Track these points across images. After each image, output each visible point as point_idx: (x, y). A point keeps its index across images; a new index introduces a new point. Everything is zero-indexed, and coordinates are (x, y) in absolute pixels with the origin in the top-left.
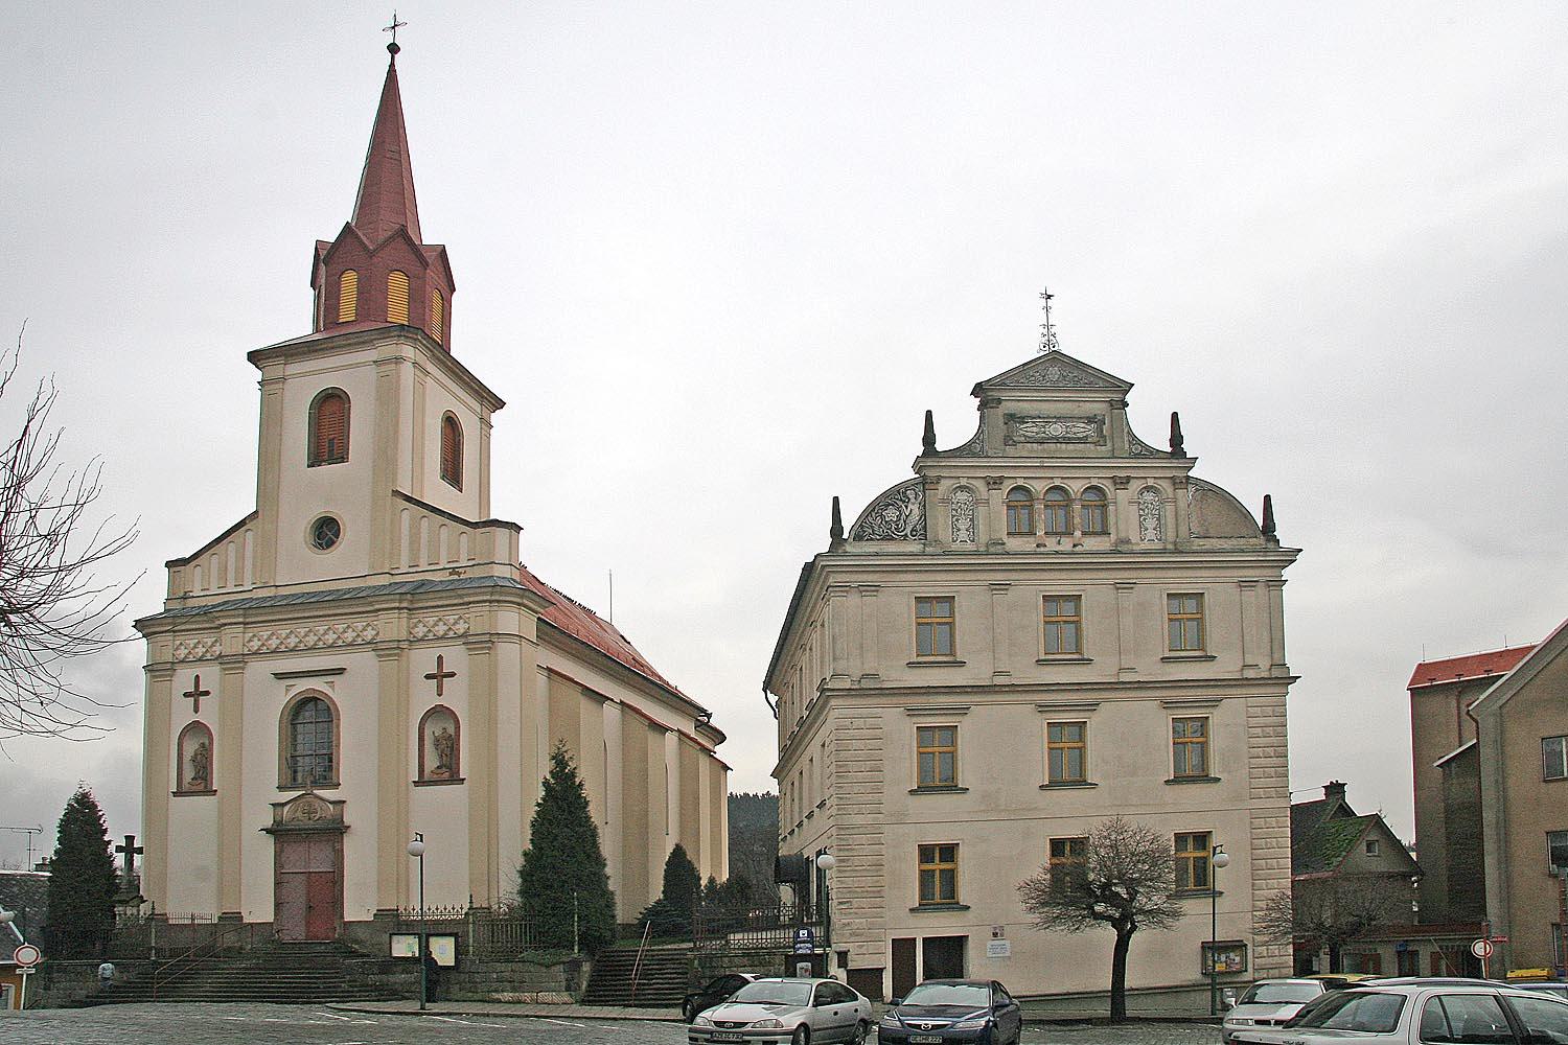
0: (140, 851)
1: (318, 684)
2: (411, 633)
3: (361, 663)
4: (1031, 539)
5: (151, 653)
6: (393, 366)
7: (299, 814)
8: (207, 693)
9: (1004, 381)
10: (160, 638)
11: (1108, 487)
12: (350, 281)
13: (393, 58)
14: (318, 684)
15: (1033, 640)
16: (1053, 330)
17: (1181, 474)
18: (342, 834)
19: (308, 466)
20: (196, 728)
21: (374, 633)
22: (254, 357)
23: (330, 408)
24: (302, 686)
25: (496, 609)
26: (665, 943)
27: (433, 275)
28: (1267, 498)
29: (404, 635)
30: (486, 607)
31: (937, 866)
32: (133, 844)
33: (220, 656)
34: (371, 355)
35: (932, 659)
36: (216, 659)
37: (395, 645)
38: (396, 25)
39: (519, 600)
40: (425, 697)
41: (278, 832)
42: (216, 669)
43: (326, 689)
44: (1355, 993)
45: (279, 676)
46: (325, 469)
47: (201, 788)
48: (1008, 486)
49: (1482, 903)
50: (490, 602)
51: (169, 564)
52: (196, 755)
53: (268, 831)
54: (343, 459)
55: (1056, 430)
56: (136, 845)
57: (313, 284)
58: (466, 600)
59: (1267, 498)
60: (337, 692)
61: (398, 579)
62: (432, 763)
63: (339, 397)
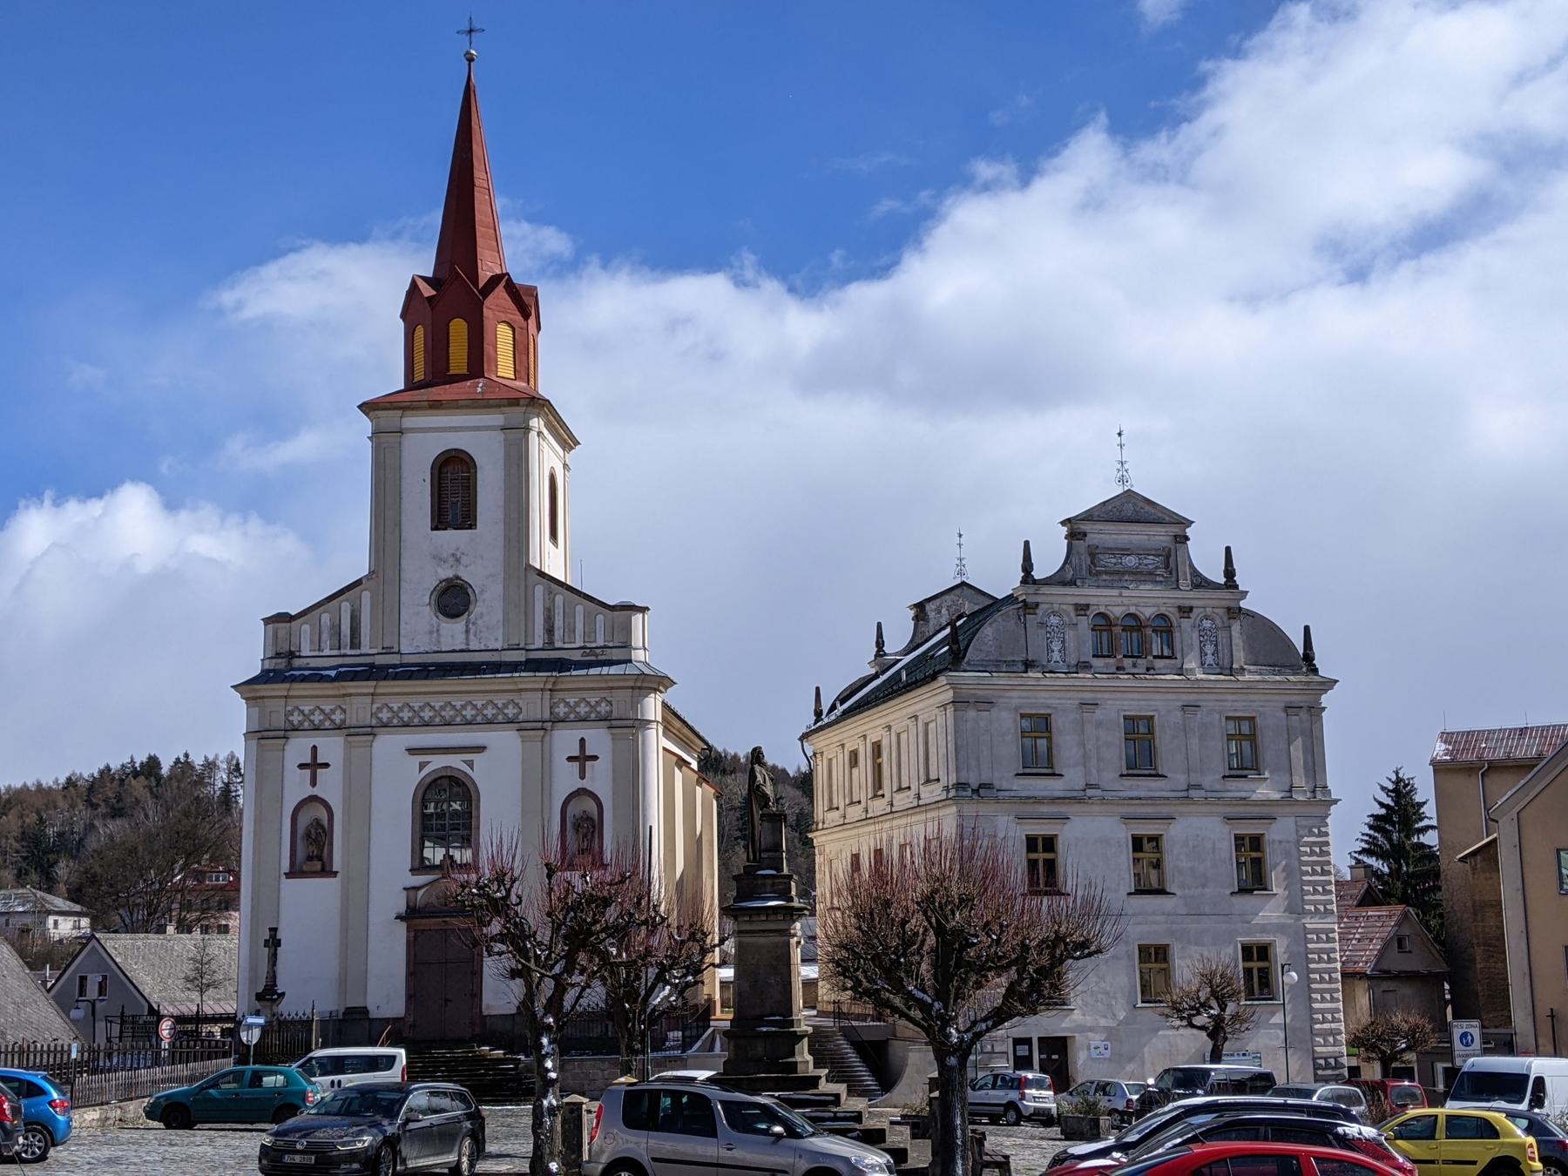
1: (456, 761)
3: (504, 744)
4: (1111, 661)
9: (1088, 516)
13: (470, 65)
15: (1009, 749)
16: (1126, 466)
17: (1232, 604)
22: (367, 407)
24: (438, 762)
28: (1307, 629)
29: (547, 715)
31: (1041, 856)
35: (1034, 771)
38: (471, 31)
40: (566, 780)
45: (412, 751)
49: (1506, 1013)
54: (472, 526)
55: (1130, 561)
59: (1307, 629)
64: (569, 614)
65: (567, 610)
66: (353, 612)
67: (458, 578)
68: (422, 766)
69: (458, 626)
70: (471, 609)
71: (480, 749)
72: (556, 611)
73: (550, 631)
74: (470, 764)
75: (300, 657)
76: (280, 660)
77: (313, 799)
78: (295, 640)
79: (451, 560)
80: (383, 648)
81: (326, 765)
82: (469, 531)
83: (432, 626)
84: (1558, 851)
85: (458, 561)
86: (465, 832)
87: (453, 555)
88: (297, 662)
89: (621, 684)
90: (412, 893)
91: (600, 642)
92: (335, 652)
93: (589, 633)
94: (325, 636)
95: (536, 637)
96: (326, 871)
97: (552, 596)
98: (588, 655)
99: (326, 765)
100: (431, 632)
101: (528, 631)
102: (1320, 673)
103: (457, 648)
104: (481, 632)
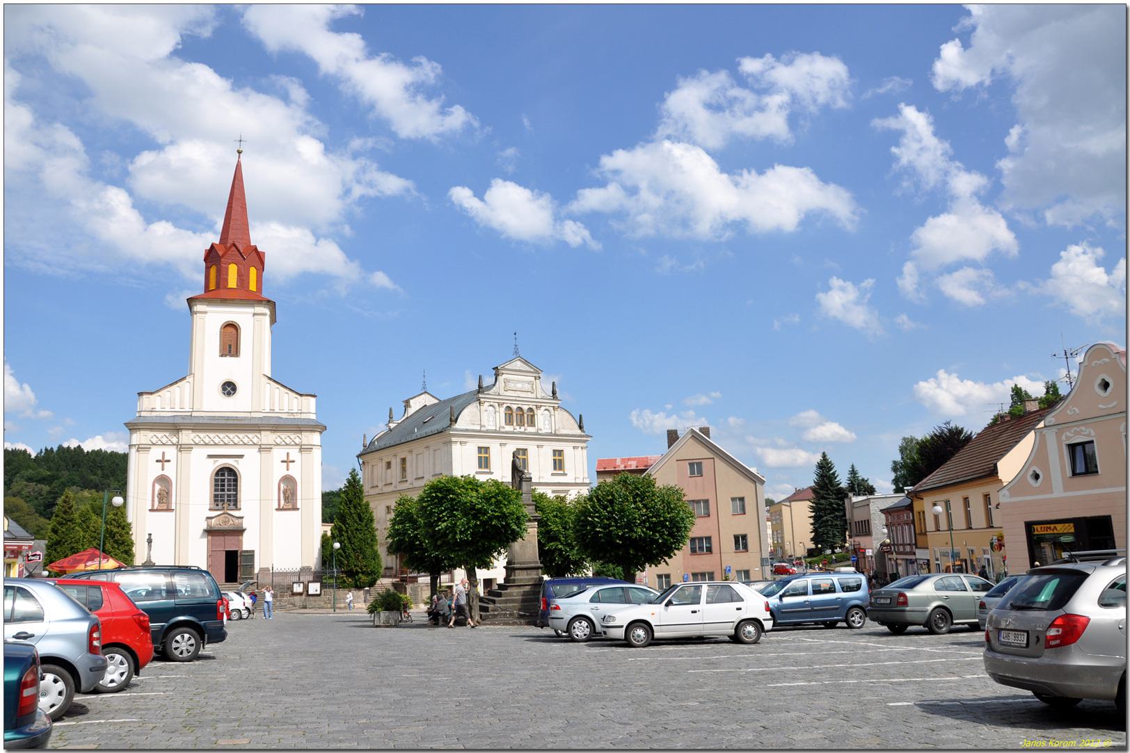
3: (251, 454)
11: (534, 408)
13: (239, 157)
24: (222, 462)
26: (360, 616)
32: (960, 40)
40: (281, 471)
41: (209, 532)
43: (235, 464)
45: (210, 456)
47: (165, 507)
48: (505, 406)
59: (580, 416)
60: (239, 466)
71: (241, 456)
84: (1028, 632)
86: (234, 493)
89: (744, 471)
90: (209, 520)
102: (776, 501)
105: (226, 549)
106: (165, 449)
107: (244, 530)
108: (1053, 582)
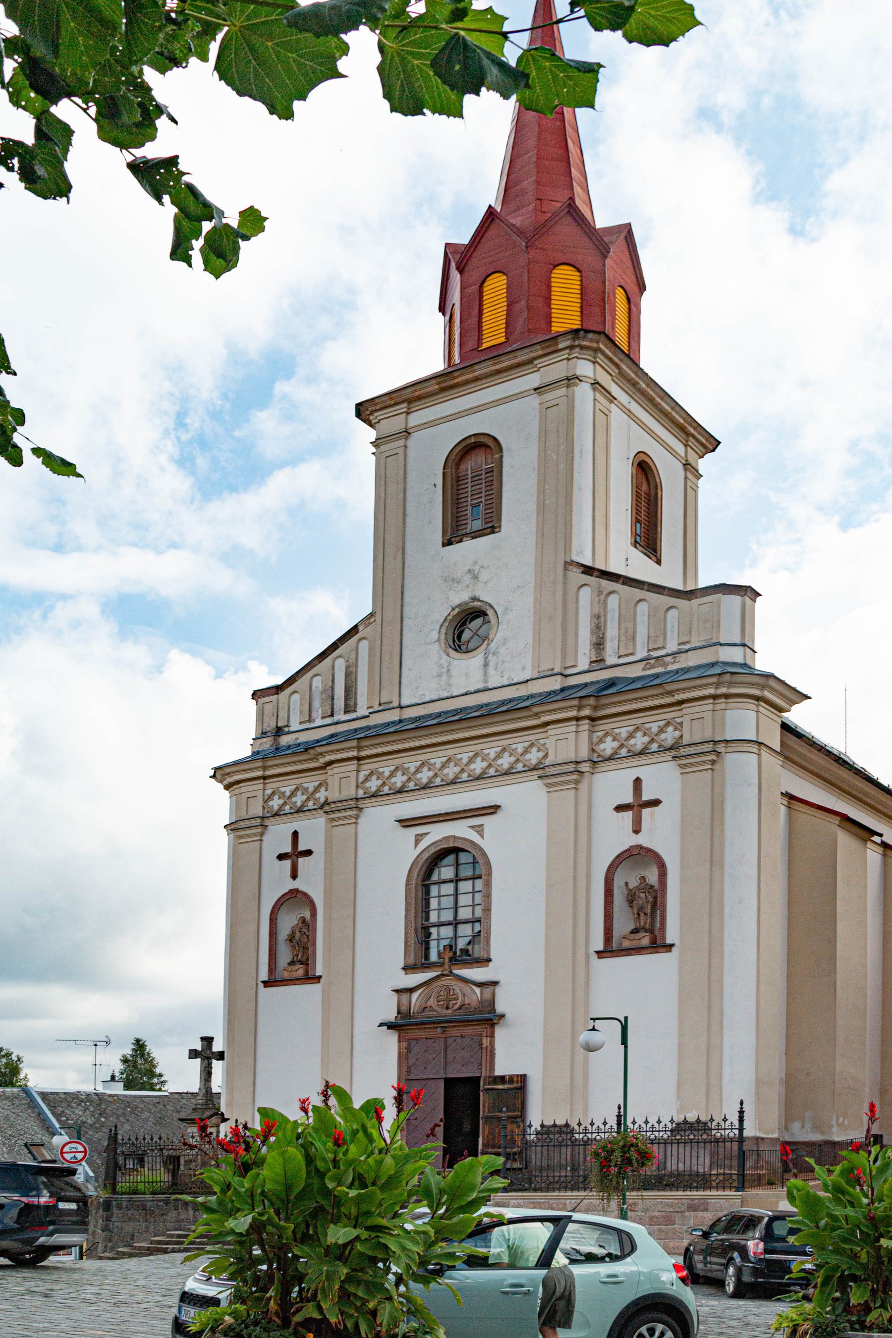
0: (221, 1056)
1: (461, 830)
2: (593, 751)
5: (236, 806)
6: (562, 391)
7: (432, 1002)
8: (308, 853)
10: (245, 788)
12: (496, 286)
14: (461, 830)
18: (493, 1025)
19: (444, 545)
20: (294, 897)
21: (541, 754)
23: (476, 462)
24: (438, 833)
25: (723, 706)
27: (614, 267)
30: (708, 705)
33: (326, 803)
34: (533, 380)
36: (321, 807)
37: (571, 768)
39: (756, 692)
42: (320, 821)
44: (552, 1209)
45: (406, 823)
46: (468, 546)
50: (715, 697)
51: (256, 695)
52: (293, 933)
53: (390, 1026)
56: (217, 1047)
57: (442, 309)
58: (678, 697)
61: (572, 681)
62: (623, 923)
63: (487, 446)
64: (627, 619)
65: (623, 612)
66: (347, 668)
67: (474, 599)
68: (418, 839)
69: (475, 661)
70: (491, 637)
71: (493, 809)
72: (609, 616)
73: (599, 645)
74: (479, 829)
75: (289, 733)
76: (264, 740)
77: (294, 893)
78: (283, 714)
79: (467, 579)
80: (380, 704)
81: (620, 808)
82: (492, 536)
83: (441, 666)
85: (475, 577)
87: (469, 571)
88: (285, 740)
90: (405, 997)
91: (672, 647)
92: (328, 721)
93: (658, 632)
94: (316, 703)
95: (580, 653)
96: (659, 945)
97: (602, 597)
98: (653, 667)
99: (620, 808)
100: (439, 675)
101: (567, 648)
103: (472, 689)
104: (503, 662)
105: (450, 1076)
106: (299, 824)
107: (403, 969)
108: (302, 1186)
